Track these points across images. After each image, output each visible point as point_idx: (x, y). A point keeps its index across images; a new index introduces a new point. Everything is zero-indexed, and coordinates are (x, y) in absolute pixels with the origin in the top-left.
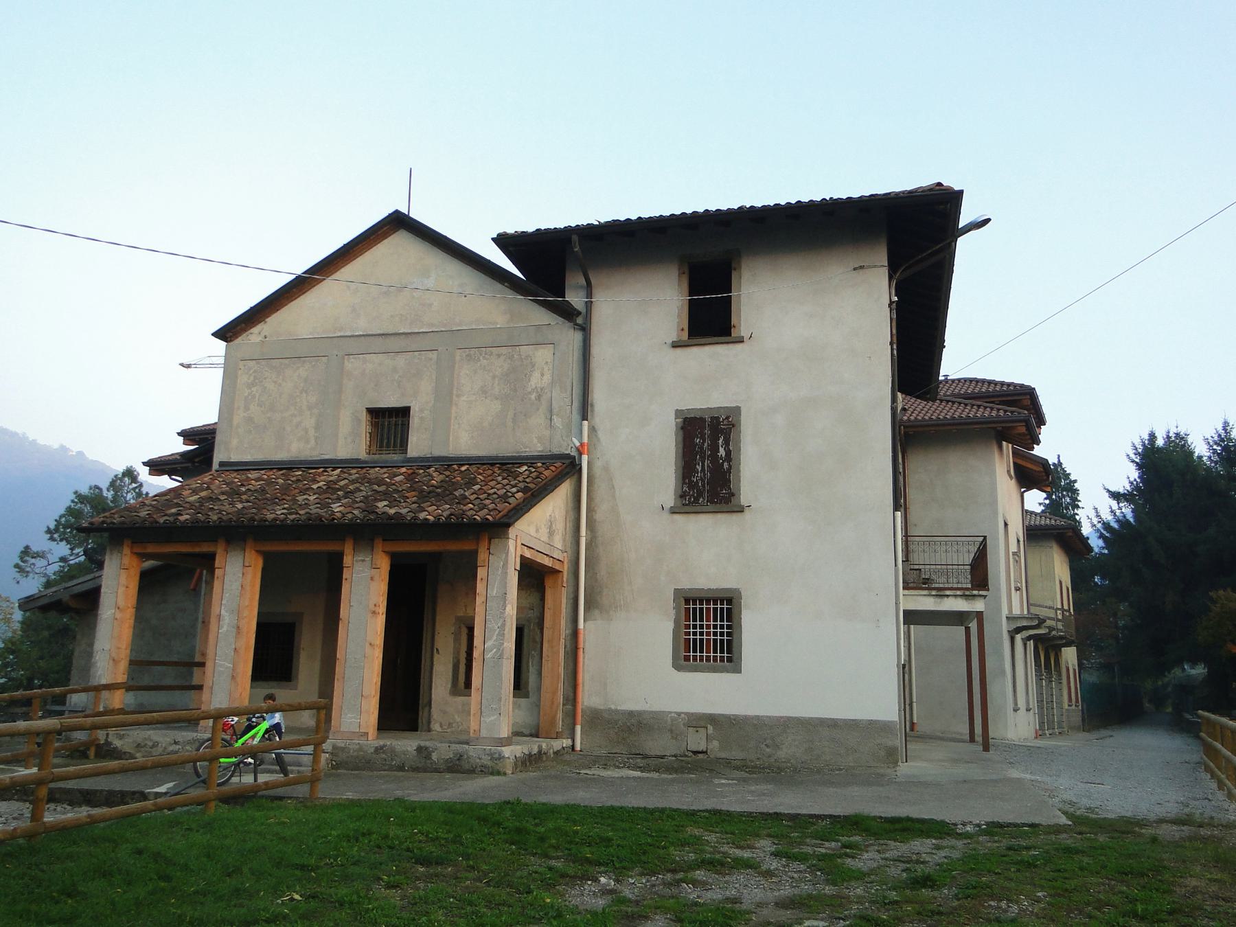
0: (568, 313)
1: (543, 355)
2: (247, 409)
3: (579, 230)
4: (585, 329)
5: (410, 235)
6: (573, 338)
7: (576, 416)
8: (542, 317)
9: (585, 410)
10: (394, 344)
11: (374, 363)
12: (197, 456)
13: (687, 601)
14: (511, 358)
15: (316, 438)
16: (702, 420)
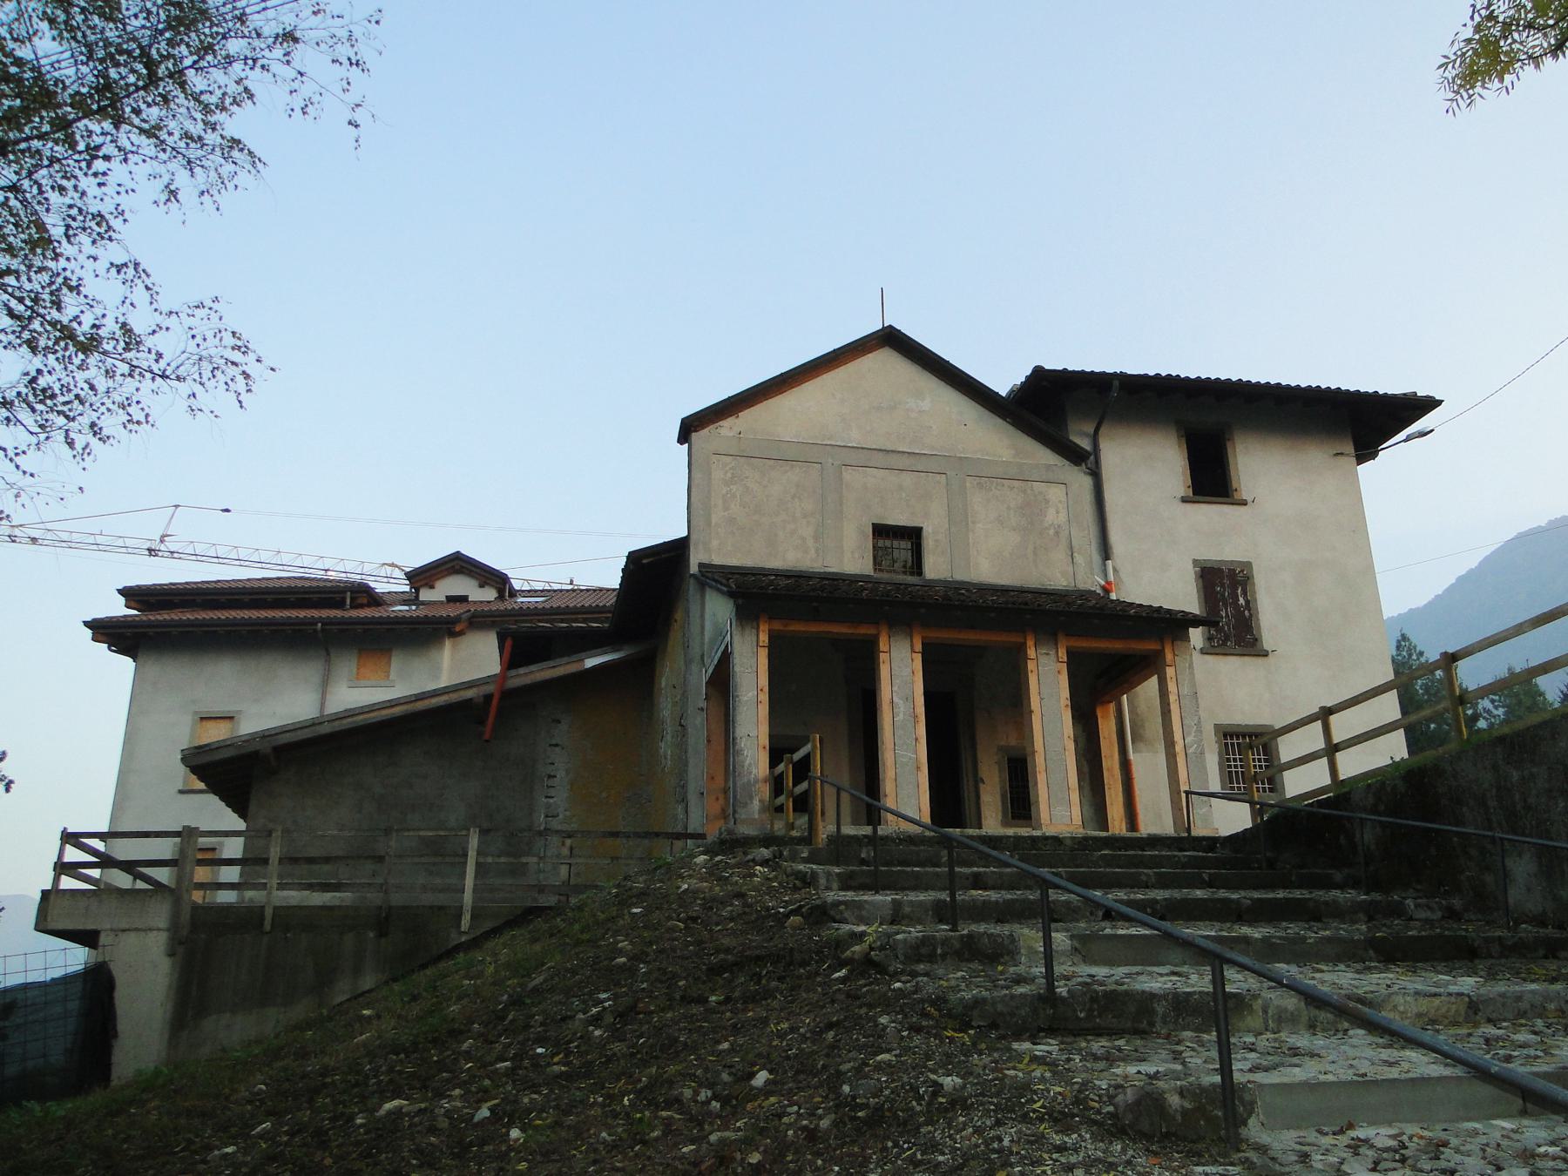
0: (1076, 456)
1: (1056, 493)
2: (726, 509)
3: (1122, 377)
4: (1096, 475)
5: (896, 354)
6: (1080, 481)
7: (1096, 558)
8: (1045, 457)
9: (1106, 551)
10: (904, 462)
11: (874, 477)
12: (647, 556)
13: (1225, 736)
14: (1024, 491)
15: (817, 550)
16: (1220, 570)
